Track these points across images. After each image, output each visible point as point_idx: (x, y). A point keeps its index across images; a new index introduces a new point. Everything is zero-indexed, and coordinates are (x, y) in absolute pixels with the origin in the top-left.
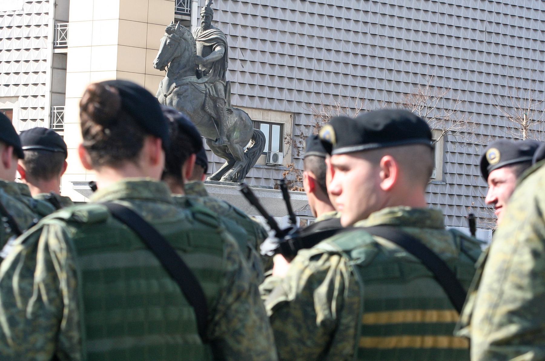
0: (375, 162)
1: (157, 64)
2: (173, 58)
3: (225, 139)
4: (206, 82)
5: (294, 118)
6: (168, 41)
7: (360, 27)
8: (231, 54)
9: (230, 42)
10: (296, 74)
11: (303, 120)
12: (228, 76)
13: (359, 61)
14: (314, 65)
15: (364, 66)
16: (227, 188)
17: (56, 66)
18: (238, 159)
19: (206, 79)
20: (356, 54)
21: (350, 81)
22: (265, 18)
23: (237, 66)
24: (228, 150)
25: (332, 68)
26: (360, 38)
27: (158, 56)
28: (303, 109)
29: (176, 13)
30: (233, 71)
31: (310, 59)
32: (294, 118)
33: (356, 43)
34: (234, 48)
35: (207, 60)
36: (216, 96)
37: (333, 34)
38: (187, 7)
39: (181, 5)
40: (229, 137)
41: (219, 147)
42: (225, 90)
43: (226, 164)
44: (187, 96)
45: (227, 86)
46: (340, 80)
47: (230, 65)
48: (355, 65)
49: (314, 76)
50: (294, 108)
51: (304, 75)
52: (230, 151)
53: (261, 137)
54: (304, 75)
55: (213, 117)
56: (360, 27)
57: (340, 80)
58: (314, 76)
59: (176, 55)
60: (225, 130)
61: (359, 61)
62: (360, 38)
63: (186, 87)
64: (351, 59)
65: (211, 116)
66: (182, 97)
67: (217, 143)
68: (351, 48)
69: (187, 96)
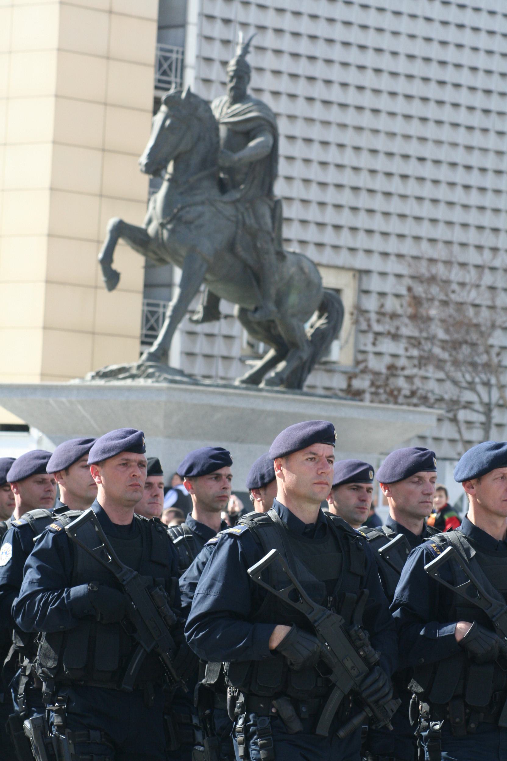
0: (461, 370)
1: (147, 165)
2: (176, 153)
3: (271, 306)
4: (238, 200)
5: (360, 280)
6: (168, 122)
7: (477, 120)
8: (284, 147)
9: (283, 127)
10: (364, 201)
11: (375, 284)
12: (280, 189)
13: (475, 179)
14: (396, 186)
15: (482, 190)
16: (278, 399)
17: (180, 31)
18: (295, 345)
19: (238, 195)
20: (468, 168)
21: (457, 215)
22: (310, 99)
23: (298, 170)
24: (275, 327)
25: (427, 191)
26: (477, 139)
27: (147, 151)
28: (375, 263)
29: (157, 88)
30: (289, 179)
31: (389, 175)
32: (360, 280)
33: (469, 148)
34: (291, 138)
35: (240, 160)
36: (256, 226)
37: (430, 131)
38: (176, 77)
39: (164, 73)
40: (279, 302)
41: (259, 324)
42: (273, 217)
43: (272, 353)
44: (201, 226)
45: (276, 208)
46: (441, 213)
47: (283, 168)
48: (467, 187)
49: (395, 205)
50: (360, 262)
51: (378, 203)
52: (281, 330)
53: (336, 305)
54: (378, 203)
55: (250, 267)
56: (477, 120)
57: (441, 213)
58: (395, 205)
59: (182, 148)
60: (273, 291)
61: (475, 179)
62: (477, 139)
63: (200, 208)
64: (460, 176)
65: (246, 266)
66: (192, 227)
67: (257, 316)
68: (460, 156)
69: (201, 226)
